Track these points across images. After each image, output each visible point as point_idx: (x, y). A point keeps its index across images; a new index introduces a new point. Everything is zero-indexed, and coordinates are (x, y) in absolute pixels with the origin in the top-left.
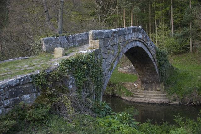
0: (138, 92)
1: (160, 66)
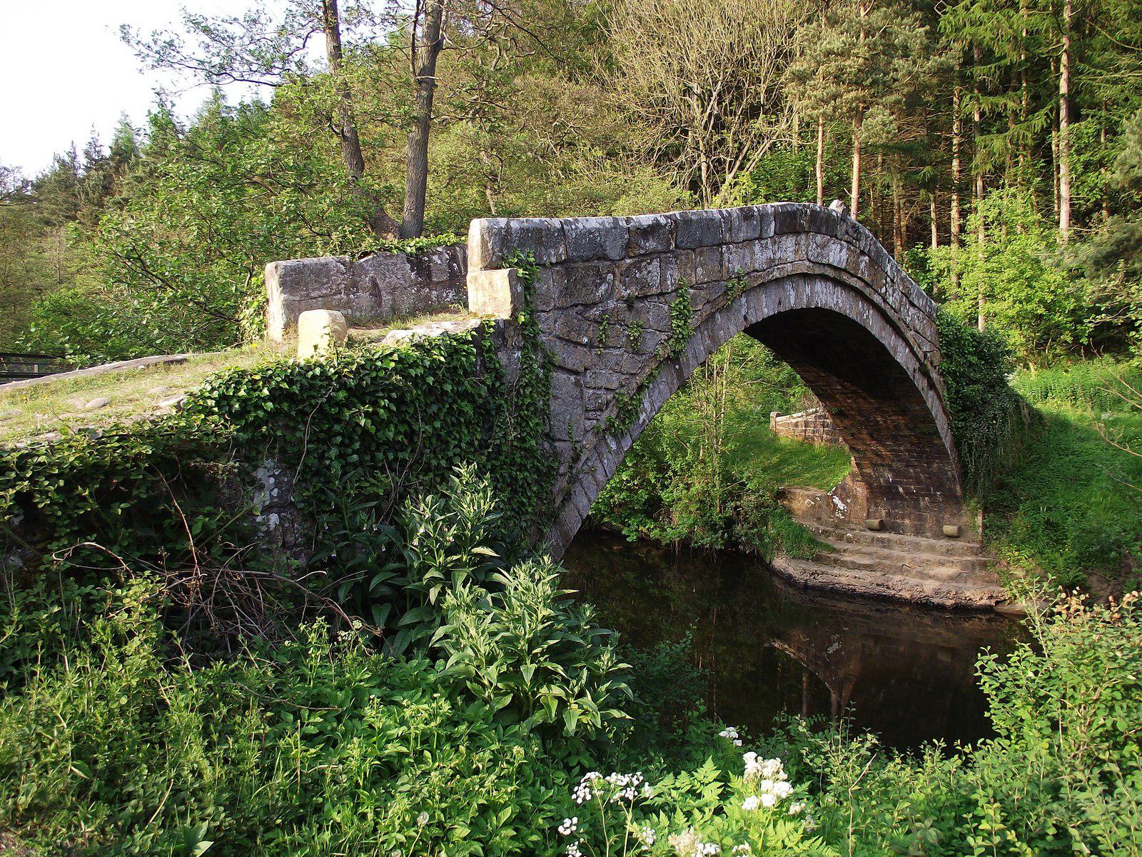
0: (849, 541)
1: (965, 409)
